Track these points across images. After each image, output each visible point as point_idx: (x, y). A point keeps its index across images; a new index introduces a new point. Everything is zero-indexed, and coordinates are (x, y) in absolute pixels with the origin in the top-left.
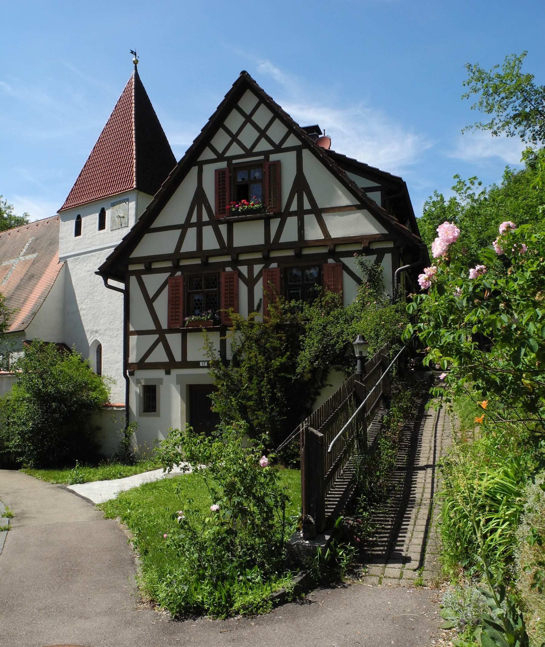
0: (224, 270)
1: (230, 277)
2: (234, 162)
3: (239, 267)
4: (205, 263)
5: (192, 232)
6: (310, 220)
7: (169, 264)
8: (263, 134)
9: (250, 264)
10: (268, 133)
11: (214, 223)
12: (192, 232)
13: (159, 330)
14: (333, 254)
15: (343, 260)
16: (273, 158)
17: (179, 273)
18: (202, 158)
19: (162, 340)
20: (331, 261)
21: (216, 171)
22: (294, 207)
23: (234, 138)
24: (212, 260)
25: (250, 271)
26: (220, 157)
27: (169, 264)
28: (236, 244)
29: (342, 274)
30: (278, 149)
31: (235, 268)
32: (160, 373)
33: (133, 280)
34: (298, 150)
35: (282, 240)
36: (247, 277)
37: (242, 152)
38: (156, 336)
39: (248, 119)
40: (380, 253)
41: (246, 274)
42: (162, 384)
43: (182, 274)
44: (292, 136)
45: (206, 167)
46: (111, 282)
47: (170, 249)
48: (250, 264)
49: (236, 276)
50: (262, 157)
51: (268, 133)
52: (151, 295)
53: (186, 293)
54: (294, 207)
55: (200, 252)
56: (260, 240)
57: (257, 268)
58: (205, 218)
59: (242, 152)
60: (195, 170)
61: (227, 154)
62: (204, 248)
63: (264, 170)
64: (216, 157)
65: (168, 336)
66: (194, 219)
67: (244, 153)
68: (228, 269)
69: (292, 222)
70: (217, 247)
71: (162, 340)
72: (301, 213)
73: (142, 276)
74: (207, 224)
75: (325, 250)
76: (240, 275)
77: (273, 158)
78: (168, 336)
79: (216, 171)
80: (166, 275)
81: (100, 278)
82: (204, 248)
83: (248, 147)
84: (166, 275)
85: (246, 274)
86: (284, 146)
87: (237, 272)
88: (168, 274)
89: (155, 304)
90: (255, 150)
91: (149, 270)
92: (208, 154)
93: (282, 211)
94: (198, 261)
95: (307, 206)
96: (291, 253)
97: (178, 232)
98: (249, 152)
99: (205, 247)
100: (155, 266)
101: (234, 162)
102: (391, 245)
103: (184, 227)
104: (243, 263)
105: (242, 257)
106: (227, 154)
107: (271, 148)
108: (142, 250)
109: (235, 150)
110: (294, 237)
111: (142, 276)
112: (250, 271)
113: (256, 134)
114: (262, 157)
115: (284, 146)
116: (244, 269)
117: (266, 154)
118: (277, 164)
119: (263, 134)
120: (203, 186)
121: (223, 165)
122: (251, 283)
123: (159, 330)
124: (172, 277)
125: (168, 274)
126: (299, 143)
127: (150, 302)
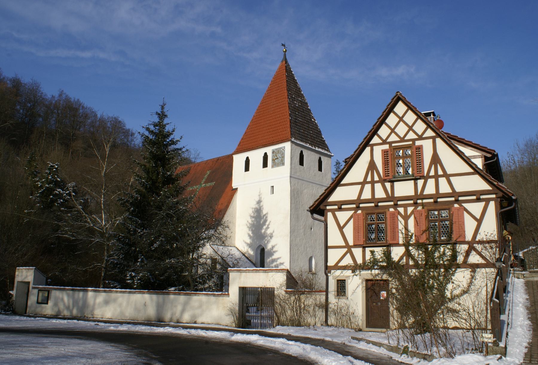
0: (389, 210)
1: (393, 214)
2: (393, 145)
3: (398, 209)
4: (377, 206)
5: (368, 187)
6: (443, 181)
7: (354, 206)
8: (411, 128)
9: (405, 206)
10: (407, 129)
11: (382, 181)
12: (368, 187)
13: (347, 246)
14: (457, 201)
15: (463, 204)
16: (418, 143)
17: (360, 212)
18: (372, 142)
19: (350, 251)
20: (456, 206)
21: (382, 150)
22: (432, 173)
23: (393, 131)
24: (380, 204)
25: (406, 211)
26: (384, 142)
27: (354, 206)
28: (396, 195)
29: (463, 213)
30: (421, 138)
31: (396, 209)
32: (349, 273)
33: (330, 215)
34: (434, 138)
35: (426, 192)
36: (403, 215)
37: (398, 139)
38: (346, 250)
39: (401, 119)
40: (488, 201)
41: (403, 213)
42: (529, 318)
43: (362, 212)
44: (429, 130)
45: (375, 148)
46: (315, 216)
47: (355, 197)
48: (405, 206)
49: (396, 214)
50: (411, 143)
51: (407, 129)
52: (342, 225)
53: (365, 223)
54: (432, 173)
55: (373, 199)
56: (412, 193)
57: (410, 209)
58: (376, 178)
59: (398, 139)
60: (368, 149)
61: (388, 141)
62: (376, 197)
63: (413, 151)
64: (382, 142)
65: (353, 250)
66: (369, 179)
67: (418, 137)
68: (392, 210)
69: (431, 182)
70: (384, 196)
71: (350, 251)
72: (436, 177)
73: (336, 212)
74: (377, 182)
75: (453, 199)
76: (399, 213)
77: (418, 143)
78: (353, 250)
79: (382, 150)
80: (351, 213)
81: (309, 213)
82: (376, 197)
83: (402, 136)
84: (351, 213)
85: (403, 213)
86: (424, 136)
87: (397, 211)
88: (353, 212)
89: (344, 230)
90: (406, 138)
91: (340, 209)
92: (375, 140)
93: (425, 175)
94: (373, 205)
95: (440, 172)
96: (432, 200)
97: (359, 187)
98: (402, 140)
99: (377, 196)
100: (343, 207)
101: (393, 145)
102: (494, 196)
103: (363, 184)
104: (401, 206)
105: (399, 203)
106: (388, 141)
107: (416, 137)
108: (335, 197)
109: (393, 138)
110: (433, 192)
111: (336, 212)
112: (406, 211)
113: (407, 129)
114: (411, 143)
115: (424, 136)
116: (401, 210)
117: (414, 140)
118: (420, 148)
119: (411, 128)
120: (374, 159)
121: (386, 147)
122: (406, 218)
123: (347, 246)
124: (355, 214)
125: (353, 212)
126: (433, 134)
127: (341, 228)
